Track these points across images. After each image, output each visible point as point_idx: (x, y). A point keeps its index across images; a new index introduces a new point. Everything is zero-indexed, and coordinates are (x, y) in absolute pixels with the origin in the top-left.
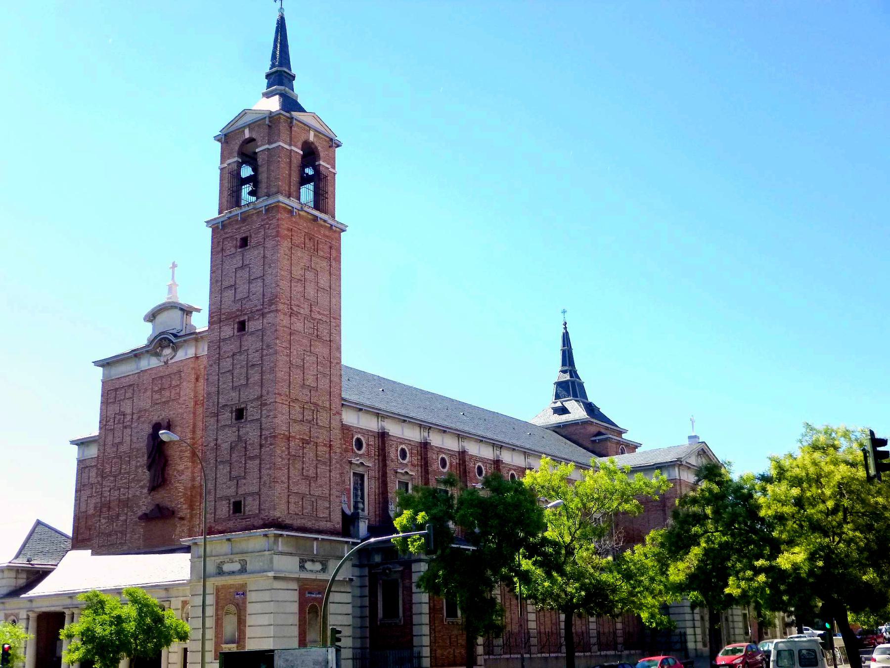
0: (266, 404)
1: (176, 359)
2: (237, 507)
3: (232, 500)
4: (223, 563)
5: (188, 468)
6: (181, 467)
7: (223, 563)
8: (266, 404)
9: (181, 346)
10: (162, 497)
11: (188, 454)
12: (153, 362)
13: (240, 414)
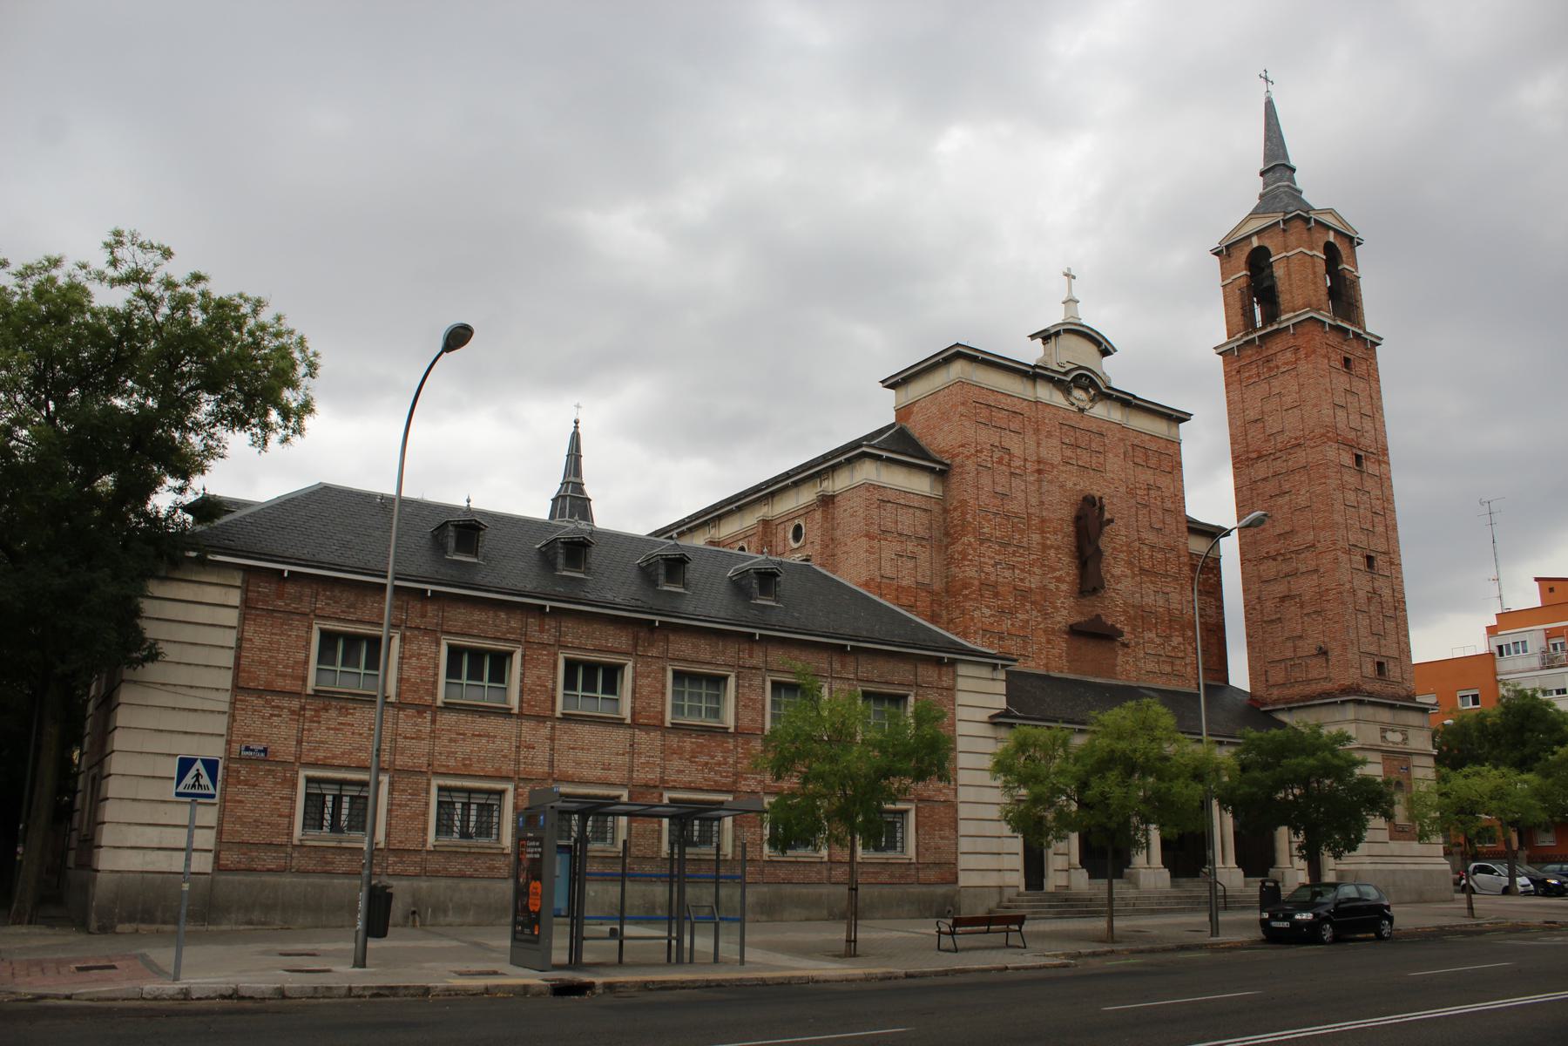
6: (1117, 571)
12: (1058, 398)
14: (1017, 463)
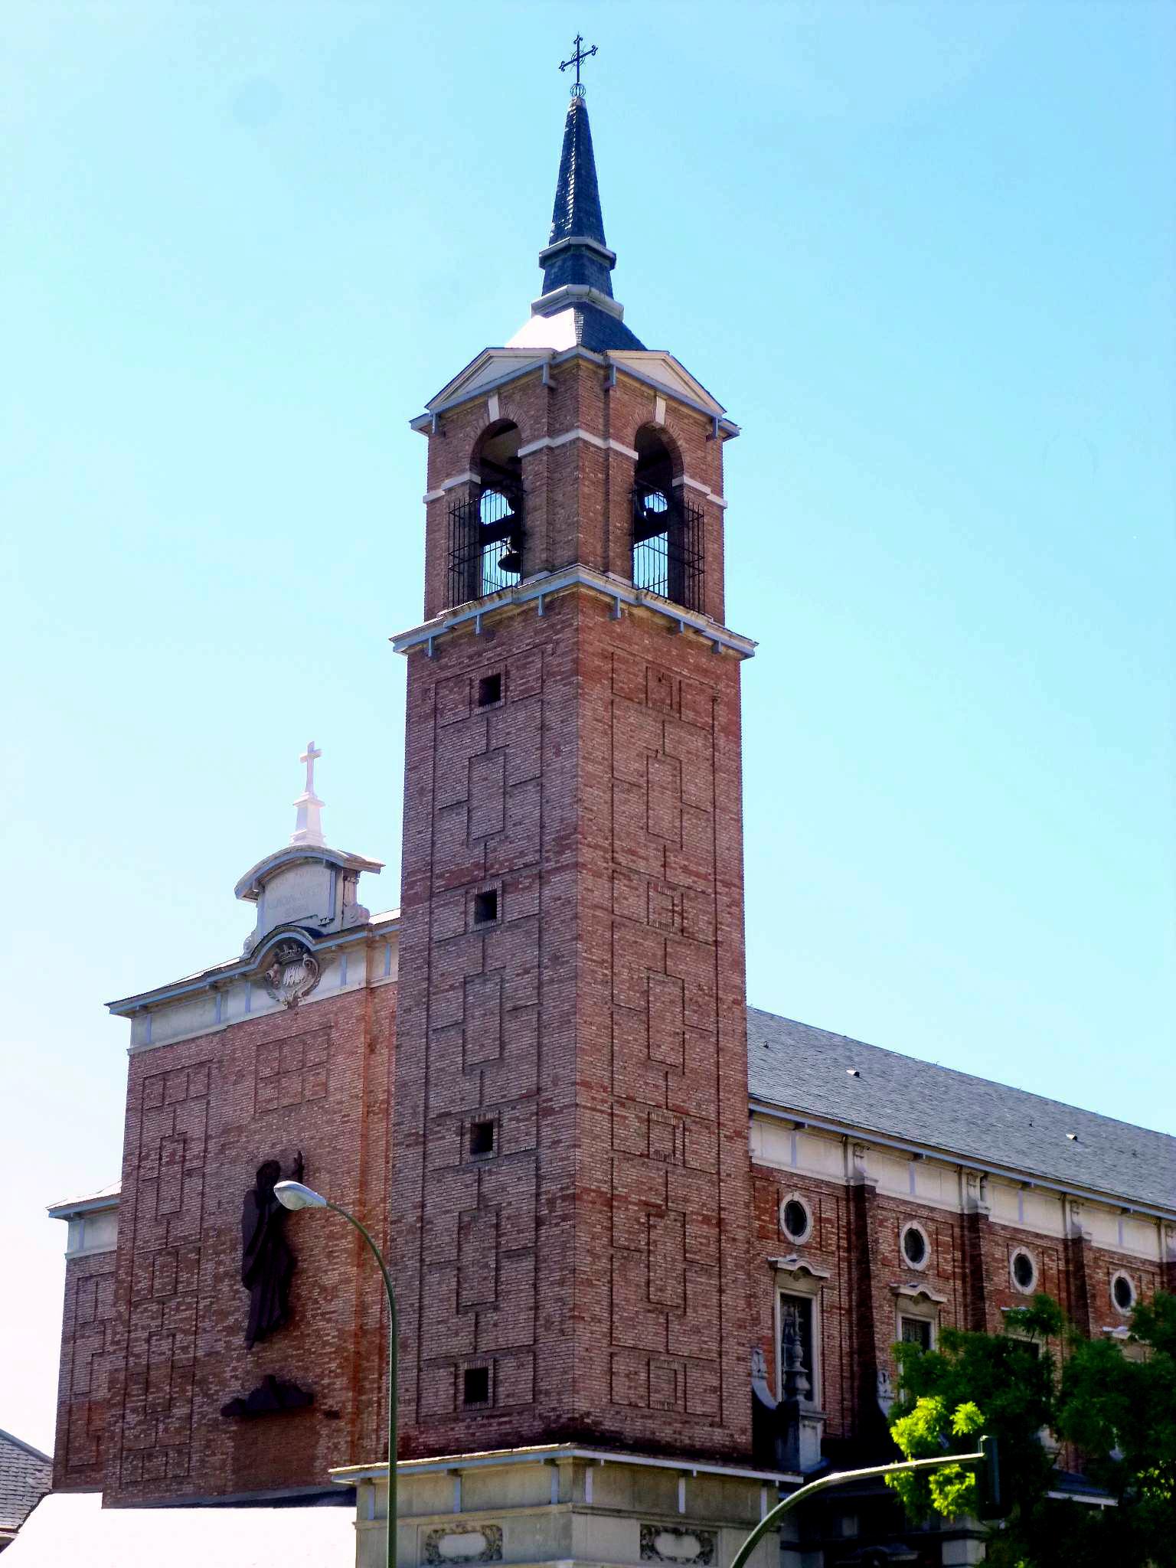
0: (550, 1111)
1: (310, 999)
2: (476, 1385)
3: (464, 1367)
4: (439, 1533)
5: (348, 1281)
6: (330, 1279)
7: (439, 1533)
8: (550, 1111)
9: (332, 961)
10: (280, 1356)
11: (348, 1243)
12: (262, 1003)
13: (483, 1138)
14: (196, 1148)
